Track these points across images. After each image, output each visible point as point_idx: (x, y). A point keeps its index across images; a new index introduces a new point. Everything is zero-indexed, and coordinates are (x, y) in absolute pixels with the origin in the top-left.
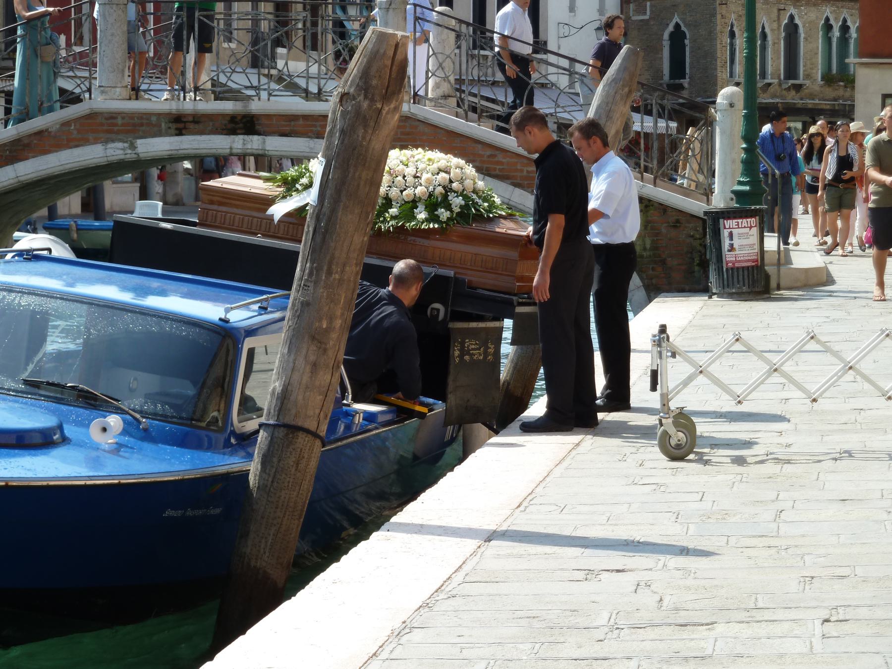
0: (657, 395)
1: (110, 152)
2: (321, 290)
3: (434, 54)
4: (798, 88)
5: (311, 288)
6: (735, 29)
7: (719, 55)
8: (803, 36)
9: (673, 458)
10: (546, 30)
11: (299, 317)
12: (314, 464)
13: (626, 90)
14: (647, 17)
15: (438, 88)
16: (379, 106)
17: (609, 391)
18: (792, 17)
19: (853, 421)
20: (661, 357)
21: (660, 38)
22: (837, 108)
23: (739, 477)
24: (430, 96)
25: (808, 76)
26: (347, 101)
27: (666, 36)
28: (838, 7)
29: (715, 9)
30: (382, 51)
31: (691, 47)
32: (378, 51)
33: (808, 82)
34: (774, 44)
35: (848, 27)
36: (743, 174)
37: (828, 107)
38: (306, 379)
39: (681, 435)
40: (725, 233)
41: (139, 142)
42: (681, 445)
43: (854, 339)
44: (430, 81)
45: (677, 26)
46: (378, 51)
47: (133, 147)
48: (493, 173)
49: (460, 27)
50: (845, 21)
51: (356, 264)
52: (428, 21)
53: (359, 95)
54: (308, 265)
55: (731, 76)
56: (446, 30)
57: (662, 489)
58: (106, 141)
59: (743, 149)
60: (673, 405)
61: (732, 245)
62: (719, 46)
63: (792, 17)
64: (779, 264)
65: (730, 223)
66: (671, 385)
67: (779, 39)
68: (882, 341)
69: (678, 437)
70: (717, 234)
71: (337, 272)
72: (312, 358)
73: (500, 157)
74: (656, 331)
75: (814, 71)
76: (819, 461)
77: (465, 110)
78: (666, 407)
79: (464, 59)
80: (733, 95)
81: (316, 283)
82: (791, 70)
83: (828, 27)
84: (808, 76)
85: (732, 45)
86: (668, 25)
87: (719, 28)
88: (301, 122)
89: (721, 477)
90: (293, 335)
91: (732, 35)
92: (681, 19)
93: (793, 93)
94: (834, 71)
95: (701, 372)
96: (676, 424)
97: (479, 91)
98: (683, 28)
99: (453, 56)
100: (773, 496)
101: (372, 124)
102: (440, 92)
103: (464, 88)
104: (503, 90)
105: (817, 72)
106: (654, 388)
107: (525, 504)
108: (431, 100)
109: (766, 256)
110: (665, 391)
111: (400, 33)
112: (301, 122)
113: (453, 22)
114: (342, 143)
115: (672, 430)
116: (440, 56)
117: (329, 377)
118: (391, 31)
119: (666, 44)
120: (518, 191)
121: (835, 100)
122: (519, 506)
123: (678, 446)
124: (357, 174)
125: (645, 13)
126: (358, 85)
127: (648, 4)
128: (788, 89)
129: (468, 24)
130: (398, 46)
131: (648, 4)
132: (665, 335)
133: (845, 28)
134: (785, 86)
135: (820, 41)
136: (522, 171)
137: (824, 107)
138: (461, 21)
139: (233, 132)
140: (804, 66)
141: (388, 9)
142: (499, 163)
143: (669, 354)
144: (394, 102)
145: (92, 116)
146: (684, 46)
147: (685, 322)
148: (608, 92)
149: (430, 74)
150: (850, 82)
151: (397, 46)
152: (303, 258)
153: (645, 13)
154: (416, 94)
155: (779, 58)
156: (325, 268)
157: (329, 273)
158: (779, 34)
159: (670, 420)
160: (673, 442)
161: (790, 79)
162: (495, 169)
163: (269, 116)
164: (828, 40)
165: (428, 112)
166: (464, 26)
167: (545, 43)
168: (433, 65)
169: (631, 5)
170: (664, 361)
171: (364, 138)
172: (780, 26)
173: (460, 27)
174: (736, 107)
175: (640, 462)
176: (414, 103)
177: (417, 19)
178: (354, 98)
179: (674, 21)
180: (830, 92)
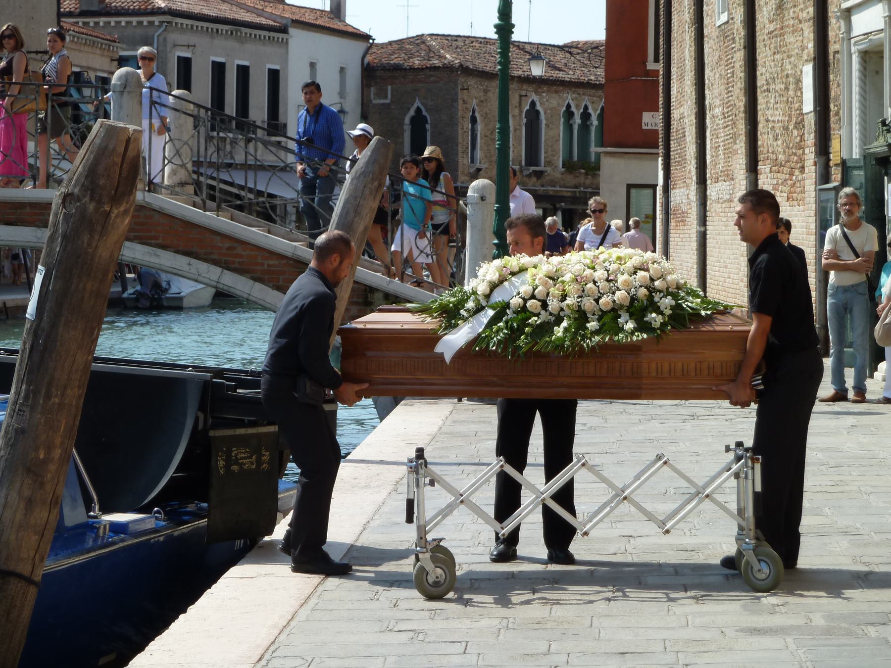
0: (413, 527)
2: (39, 416)
3: (171, 140)
4: (539, 174)
5: (27, 414)
6: (477, 114)
7: (460, 140)
8: (544, 122)
9: (431, 597)
10: (286, 112)
11: (12, 446)
12: (27, 613)
13: (376, 183)
14: (388, 101)
15: (175, 174)
16: (107, 208)
17: (284, 341)
18: (533, 104)
19: (623, 550)
20: (418, 486)
21: (402, 123)
22: (578, 195)
23: (505, 621)
24: (166, 182)
25: (548, 163)
26: (70, 203)
27: (407, 120)
28: (579, 94)
29: (456, 94)
30: (111, 147)
31: (432, 133)
32: (106, 147)
33: (549, 169)
34: (515, 130)
35: (590, 115)
37: (569, 194)
38: (19, 517)
39: (439, 571)
42: (439, 582)
43: (614, 451)
44: (166, 168)
45: (418, 110)
46: (106, 147)
48: (232, 266)
49: (199, 111)
50: (586, 108)
51: (79, 387)
52: (165, 106)
53: (84, 196)
54: (24, 387)
55: (472, 161)
56: (183, 116)
57: (421, 637)
59: (495, 244)
60: (429, 537)
62: (460, 131)
63: (533, 104)
66: (429, 514)
67: (520, 125)
68: (659, 468)
69: (436, 573)
71: (56, 396)
72: (27, 493)
73: (239, 250)
74: (413, 454)
75: (556, 158)
76: (591, 602)
77: (202, 200)
78: (423, 540)
79: (202, 141)
80: (484, 187)
81: (32, 408)
82: (532, 156)
83: (569, 114)
84: (548, 163)
85: (473, 131)
86: (409, 109)
87: (460, 113)
88: (28, 210)
89: (484, 622)
90: (5, 467)
91: (474, 120)
92: (422, 104)
93: (534, 179)
94: (576, 158)
95: (462, 502)
96: (434, 559)
97: (218, 175)
98: (424, 113)
99: (190, 143)
100: (544, 648)
101: (99, 228)
102: (176, 179)
103: (202, 170)
104: (243, 173)
105: (558, 159)
106: (410, 519)
107: (267, 656)
108: (167, 188)
110: (422, 523)
111: (132, 127)
112: (28, 210)
113: (192, 106)
114: (64, 250)
115: (429, 566)
116: (176, 142)
117: (46, 515)
118: (121, 125)
119: (407, 128)
120: (258, 285)
121: (576, 187)
122: (260, 659)
123: (436, 584)
124: (81, 285)
125: (386, 97)
126: (83, 185)
127: (389, 87)
128: (529, 176)
129: (207, 109)
130: (131, 141)
131: (389, 87)
132: (422, 461)
133: (586, 116)
134: (526, 173)
135: (561, 128)
136: (262, 264)
137: (566, 194)
138: (198, 106)
140: (545, 153)
141: (122, 93)
142: (238, 256)
143: (427, 480)
144: (124, 204)
146: (425, 131)
147: (435, 429)
149: (166, 162)
150: (594, 169)
151: (128, 141)
152: (18, 379)
153: (386, 97)
154: (151, 182)
155: (520, 144)
156: (43, 391)
157: (48, 397)
158: (521, 119)
159: (428, 555)
160: (431, 579)
161: (531, 166)
162: (234, 263)
164: (569, 127)
165: (164, 201)
166: (202, 111)
167: (285, 125)
168: (170, 151)
169: (372, 89)
170: (421, 490)
171: (89, 245)
172: (521, 111)
173: (199, 111)
174: (487, 201)
175: (394, 602)
176: (149, 191)
177: (153, 103)
178: (79, 200)
179: (415, 105)
180: (571, 179)
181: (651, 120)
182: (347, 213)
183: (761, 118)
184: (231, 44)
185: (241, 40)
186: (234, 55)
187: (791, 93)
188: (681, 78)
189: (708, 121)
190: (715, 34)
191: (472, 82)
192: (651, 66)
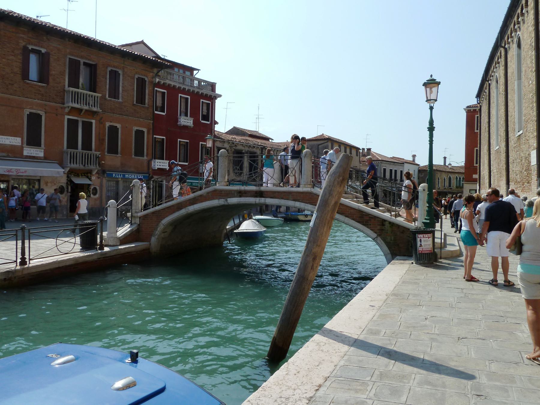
1: (220, 202)
13: (341, 178)
36: (427, 216)
40: (418, 240)
41: (228, 199)
47: (227, 201)
58: (219, 199)
61: (421, 244)
64: (441, 248)
65: (421, 236)
70: (415, 239)
82: (450, 185)
83: (457, 178)
109: (436, 244)
120: (347, 218)
139: (256, 197)
145: (215, 191)
148: (330, 179)
163: (267, 192)
164: (457, 180)
181: (475, 176)
182: (325, 195)
183: (510, 170)
184: (394, 166)
185: (395, 165)
186: (394, 168)
187: (523, 162)
188: (484, 165)
189: (492, 174)
190: (494, 152)
191: (438, 172)
192: (475, 165)
